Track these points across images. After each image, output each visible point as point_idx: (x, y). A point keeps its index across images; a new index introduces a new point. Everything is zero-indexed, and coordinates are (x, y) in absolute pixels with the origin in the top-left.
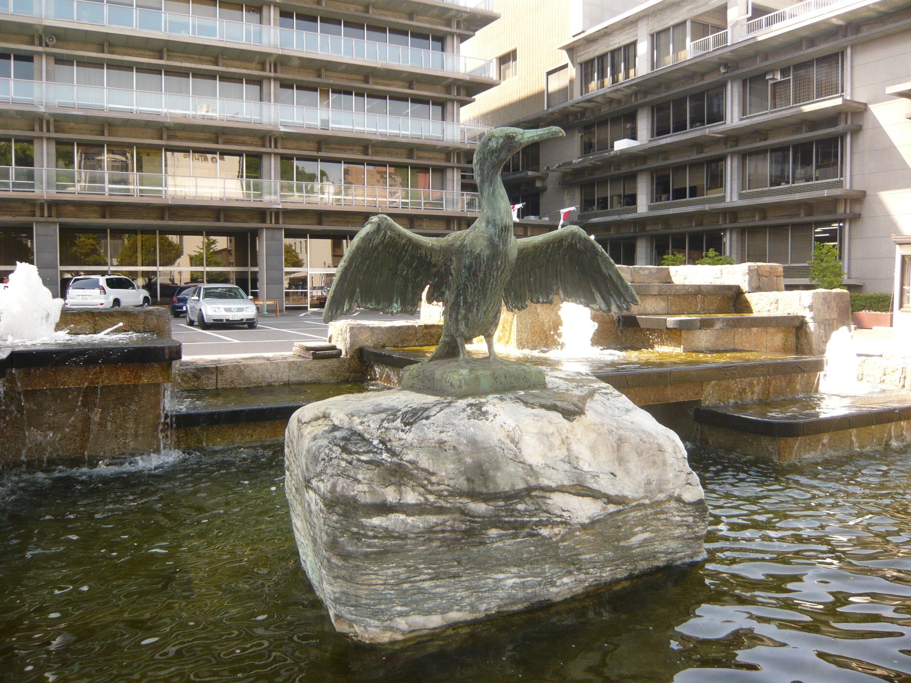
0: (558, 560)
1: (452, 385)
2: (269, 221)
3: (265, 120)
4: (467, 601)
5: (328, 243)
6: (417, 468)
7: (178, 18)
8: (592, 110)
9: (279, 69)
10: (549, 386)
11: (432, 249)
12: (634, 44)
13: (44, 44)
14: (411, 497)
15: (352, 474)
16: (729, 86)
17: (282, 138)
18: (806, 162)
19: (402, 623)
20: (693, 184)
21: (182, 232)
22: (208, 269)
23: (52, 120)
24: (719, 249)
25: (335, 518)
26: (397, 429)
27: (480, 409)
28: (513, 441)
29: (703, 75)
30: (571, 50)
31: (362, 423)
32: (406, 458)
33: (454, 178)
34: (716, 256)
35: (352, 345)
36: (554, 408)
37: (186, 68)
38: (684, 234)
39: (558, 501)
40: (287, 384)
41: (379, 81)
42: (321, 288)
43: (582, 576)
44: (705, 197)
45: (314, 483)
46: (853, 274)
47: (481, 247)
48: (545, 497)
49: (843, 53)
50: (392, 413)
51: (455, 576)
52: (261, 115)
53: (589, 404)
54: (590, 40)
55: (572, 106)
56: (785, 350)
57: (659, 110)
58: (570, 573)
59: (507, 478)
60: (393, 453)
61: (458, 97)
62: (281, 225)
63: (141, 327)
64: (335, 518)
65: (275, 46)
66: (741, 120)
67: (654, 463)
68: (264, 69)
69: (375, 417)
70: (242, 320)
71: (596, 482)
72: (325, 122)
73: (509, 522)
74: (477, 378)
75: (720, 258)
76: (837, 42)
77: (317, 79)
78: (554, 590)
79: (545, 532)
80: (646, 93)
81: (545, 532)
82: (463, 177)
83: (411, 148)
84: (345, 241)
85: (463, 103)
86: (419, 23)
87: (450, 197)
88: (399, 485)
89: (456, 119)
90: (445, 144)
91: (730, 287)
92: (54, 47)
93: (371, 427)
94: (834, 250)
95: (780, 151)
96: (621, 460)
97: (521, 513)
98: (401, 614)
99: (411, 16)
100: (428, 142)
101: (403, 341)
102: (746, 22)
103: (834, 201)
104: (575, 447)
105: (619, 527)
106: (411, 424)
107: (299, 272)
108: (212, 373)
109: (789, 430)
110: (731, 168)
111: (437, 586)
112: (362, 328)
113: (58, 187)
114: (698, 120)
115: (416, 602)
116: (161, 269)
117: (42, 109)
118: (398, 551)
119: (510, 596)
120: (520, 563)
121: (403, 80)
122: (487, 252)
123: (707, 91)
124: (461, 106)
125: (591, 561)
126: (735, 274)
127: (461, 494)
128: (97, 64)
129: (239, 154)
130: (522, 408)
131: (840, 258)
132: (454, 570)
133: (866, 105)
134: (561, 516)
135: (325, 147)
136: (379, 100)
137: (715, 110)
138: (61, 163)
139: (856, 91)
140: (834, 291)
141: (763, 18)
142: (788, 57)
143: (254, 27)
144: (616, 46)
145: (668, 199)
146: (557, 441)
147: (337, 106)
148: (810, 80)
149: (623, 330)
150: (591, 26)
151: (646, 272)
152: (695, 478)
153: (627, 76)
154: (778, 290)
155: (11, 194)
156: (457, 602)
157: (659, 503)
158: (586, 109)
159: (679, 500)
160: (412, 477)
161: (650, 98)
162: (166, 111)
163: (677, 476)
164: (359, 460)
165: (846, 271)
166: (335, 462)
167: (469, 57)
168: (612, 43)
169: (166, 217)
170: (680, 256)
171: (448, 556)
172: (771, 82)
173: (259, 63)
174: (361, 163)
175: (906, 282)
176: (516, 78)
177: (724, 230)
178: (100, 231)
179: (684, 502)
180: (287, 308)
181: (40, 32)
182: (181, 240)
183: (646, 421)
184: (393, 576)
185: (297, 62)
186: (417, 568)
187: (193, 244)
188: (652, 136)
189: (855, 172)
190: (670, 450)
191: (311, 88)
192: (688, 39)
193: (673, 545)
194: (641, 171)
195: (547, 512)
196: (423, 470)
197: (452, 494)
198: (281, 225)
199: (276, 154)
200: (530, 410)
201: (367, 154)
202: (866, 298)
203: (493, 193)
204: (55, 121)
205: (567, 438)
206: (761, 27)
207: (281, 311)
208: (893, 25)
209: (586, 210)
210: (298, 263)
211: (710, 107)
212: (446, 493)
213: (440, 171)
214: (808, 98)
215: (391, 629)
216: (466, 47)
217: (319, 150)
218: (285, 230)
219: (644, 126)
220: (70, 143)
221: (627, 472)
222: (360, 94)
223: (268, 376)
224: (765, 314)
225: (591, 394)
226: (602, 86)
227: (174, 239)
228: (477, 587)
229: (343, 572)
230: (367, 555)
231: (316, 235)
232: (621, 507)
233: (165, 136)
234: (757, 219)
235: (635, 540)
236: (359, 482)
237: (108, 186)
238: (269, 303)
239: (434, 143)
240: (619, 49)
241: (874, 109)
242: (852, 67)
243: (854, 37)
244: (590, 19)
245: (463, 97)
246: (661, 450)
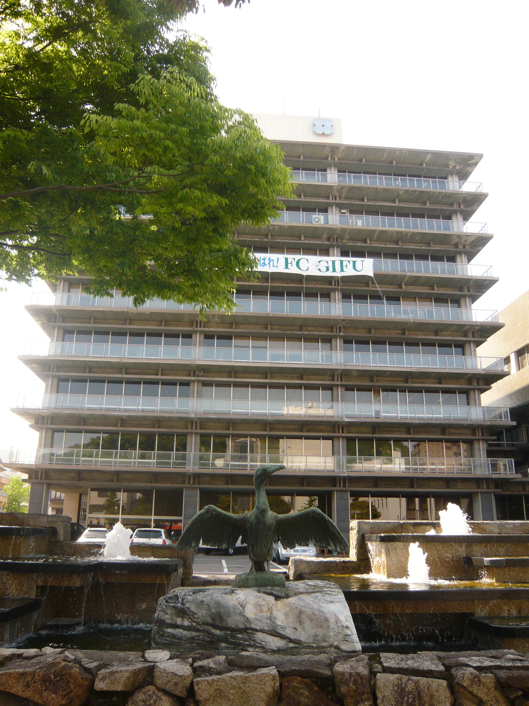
2: (338, 486)
5: (404, 500)
6: (189, 611)
9: (343, 379)
11: (236, 520)
13: (196, 375)
14: (186, 623)
17: (347, 426)
23: (198, 422)
25: (156, 628)
28: (242, 606)
32: (186, 606)
33: (481, 448)
37: (282, 383)
39: (260, 636)
41: (416, 380)
47: (253, 519)
48: (254, 634)
59: (233, 621)
61: (478, 387)
67: (322, 626)
68: (333, 380)
71: (283, 631)
72: (377, 412)
73: (231, 642)
84: (428, 499)
85: (483, 391)
88: (183, 617)
90: (470, 423)
92: (202, 376)
96: (301, 623)
99: (436, 333)
100: (456, 422)
104: (275, 613)
113: (201, 464)
117: (192, 416)
121: (433, 378)
122: (255, 521)
127: (208, 624)
128: (227, 385)
134: (260, 644)
138: (203, 449)
146: (265, 609)
151: (511, 526)
155: (171, 470)
160: (187, 614)
163: (336, 635)
164: (169, 605)
166: (162, 606)
178: (227, 493)
179: (341, 650)
181: (195, 368)
182: (292, 500)
185: (356, 373)
195: (254, 641)
196: (192, 611)
199: (342, 437)
201: (410, 434)
204: (201, 422)
205: (271, 608)
212: (201, 623)
213: (470, 443)
216: (481, 350)
217: (374, 433)
218: (351, 492)
220: (209, 436)
221: (304, 629)
232: (297, 645)
233: (268, 429)
239: (460, 422)
246: (326, 620)
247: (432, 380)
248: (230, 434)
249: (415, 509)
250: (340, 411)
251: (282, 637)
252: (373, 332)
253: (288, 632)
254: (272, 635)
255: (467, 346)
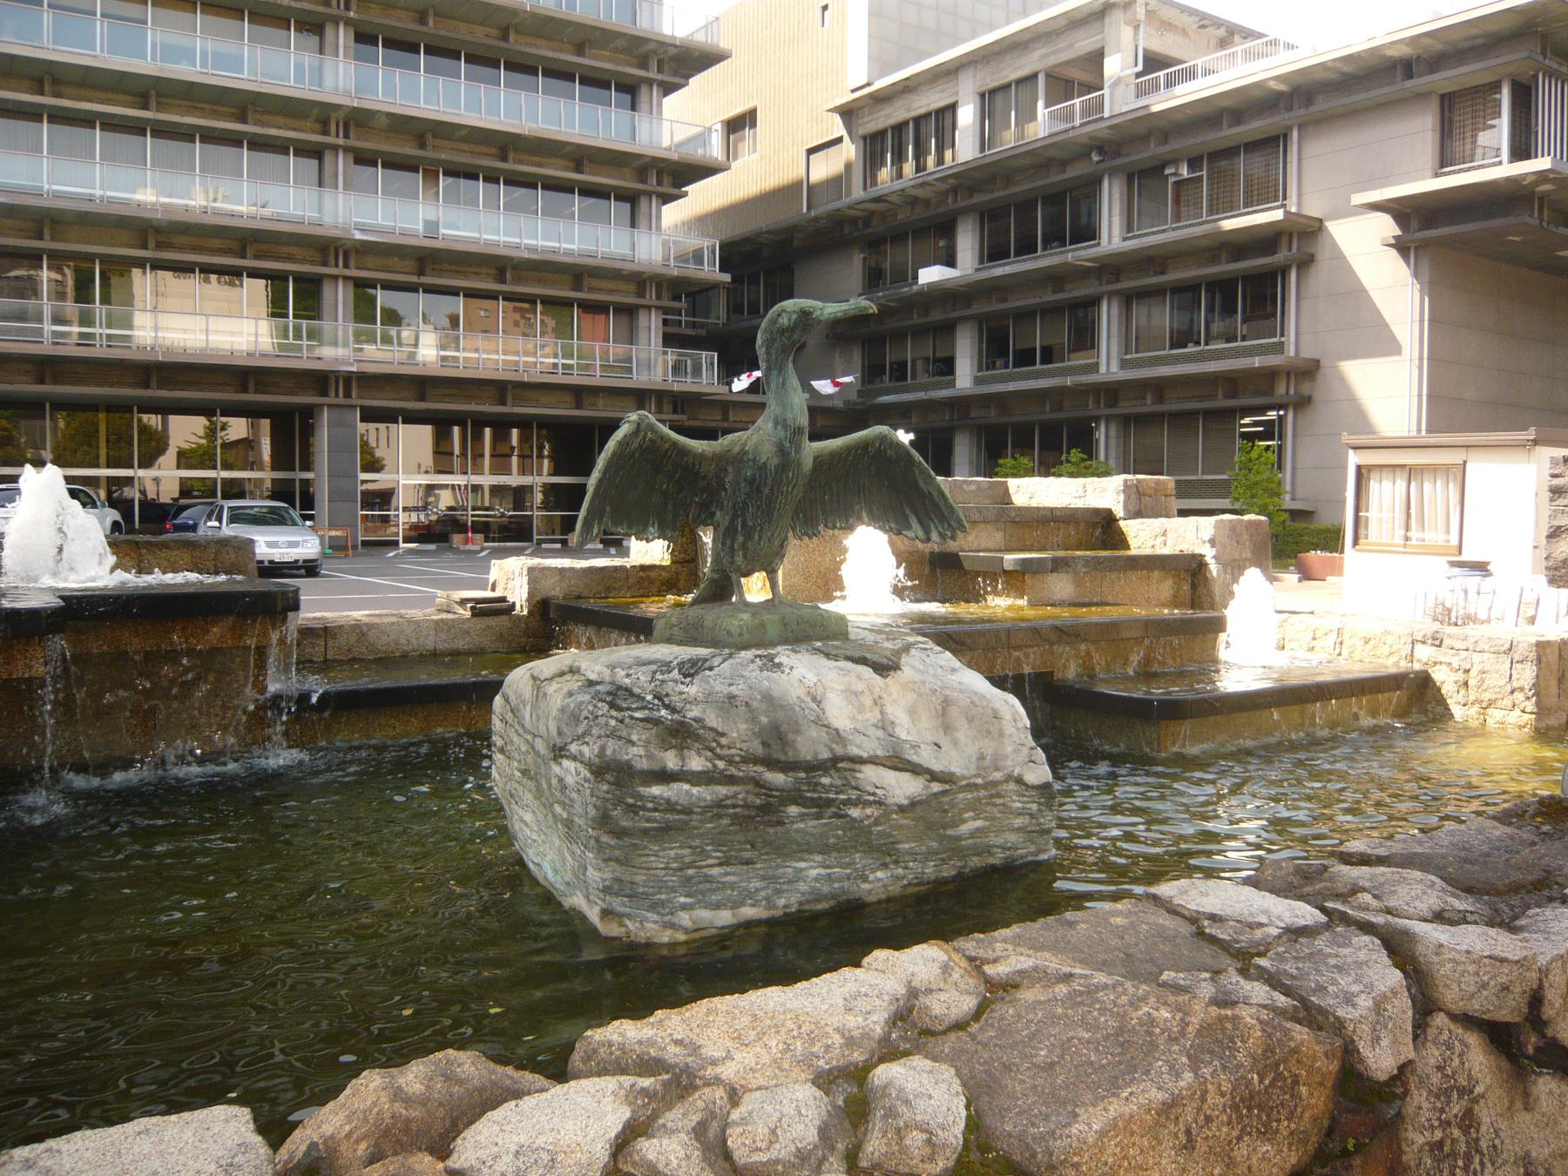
0: (871, 849)
1: (729, 633)
2: (333, 393)
3: (328, 219)
4: (763, 893)
5: (425, 432)
6: (704, 727)
7: (177, 39)
8: (882, 215)
10: (852, 637)
11: (702, 456)
12: (953, 107)
14: (696, 763)
15: (624, 734)
16: (1106, 184)
18: (1229, 309)
19: (685, 919)
20: (1047, 343)
21: (167, 409)
22: (225, 474)
24: (1089, 449)
25: (605, 787)
26: (676, 681)
27: (772, 660)
28: (814, 699)
29: (1064, 164)
30: (848, 113)
31: (628, 676)
32: (691, 714)
33: (651, 326)
34: (1083, 460)
35: (531, 595)
36: (862, 661)
38: (1032, 424)
39: (871, 775)
40: (435, 654)
42: (416, 509)
43: (900, 871)
44: (1066, 364)
45: (574, 748)
46: (1300, 493)
47: (768, 454)
49: (1285, 136)
50: (666, 666)
51: (748, 862)
52: (320, 211)
53: (904, 659)
54: (881, 99)
55: (850, 207)
56: (1175, 603)
57: (991, 218)
58: (885, 866)
59: (811, 744)
60: (673, 710)
61: (659, 189)
62: (354, 400)
63: (210, 565)
64: (605, 787)
65: (347, 94)
66: (1125, 239)
67: (989, 732)
68: (326, 132)
69: (644, 669)
70: (297, 561)
71: (916, 753)
72: (432, 226)
74: (762, 625)
75: (1089, 466)
76: (1277, 118)
77: (419, 152)
78: (865, 886)
79: (855, 813)
80: (972, 190)
81: (855, 813)
82: (665, 322)
83: (578, 274)
85: (667, 199)
86: (592, 61)
87: (643, 355)
88: (681, 749)
89: (654, 224)
90: (636, 268)
91: (1097, 511)
93: (641, 680)
94: (1270, 454)
95: (1186, 293)
96: (947, 728)
97: (827, 789)
98: (684, 907)
100: (608, 264)
101: (608, 589)
102: (1133, 80)
103: (1271, 375)
104: (889, 710)
105: (945, 811)
106: (692, 675)
107: (381, 480)
108: (319, 637)
109: (1173, 711)
110: (1108, 318)
111: (727, 874)
112: (544, 570)
114: (1055, 238)
115: (700, 890)
116: (141, 473)
118: (681, 828)
119: (813, 891)
120: (825, 850)
122: (775, 462)
123: (1071, 190)
124: (665, 203)
125: (911, 853)
126: (1102, 492)
127: (756, 761)
129: (254, 274)
130: (823, 661)
131: (1280, 468)
132: (747, 855)
133: (1320, 221)
134: (874, 794)
135: (430, 268)
136: (524, 190)
137: (1084, 220)
139: (1306, 198)
140: (1247, 517)
141: (1161, 73)
142: (1199, 139)
143: (309, 59)
144: (923, 111)
145: (1006, 367)
146: (868, 702)
147: (452, 198)
148: (1234, 175)
149: (938, 572)
150: (882, 76)
151: (973, 487)
152: (1040, 755)
153: (940, 160)
154: (1168, 516)
156: (750, 895)
157: (995, 783)
158: (872, 213)
159: (1019, 781)
160: (698, 738)
161: (978, 199)
162: (153, 199)
164: (632, 717)
165: (1288, 487)
166: (602, 720)
167: (680, 119)
168: (915, 105)
169: (154, 383)
170: (1025, 461)
171: (740, 837)
172: (1172, 180)
173: (317, 121)
174: (492, 296)
175: (1363, 507)
176: (754, 156)
177: (1097, 419)
180: (365, 543)
182: (165, 423)
183: (977, 682)
184: (678, 858)
185: (384, 121)
186: (703, 851)
187: (186, 430)
188: (981, 262)
189: (1303, 328)
190: (1008, 716)
191: (409, 166)
192: (1040, 104)
193: (1012, 838)
194: (964, 319)
196: (711, 729)
197: (745, 760)
198: (354, 400)
199: (346, 278)
200: (833, 663)
201: (503, 282)
202: (1319, 532)
203: (784, 383)
206: (1158, 88)
207: (355, 547)
208: (1364, 96)
209: (870, 382)
210: (373, 465)
211: (1076, 215)
213: (628, 312)
214: (1230, 208)
215: (672, 926)
216: (672, 103)
217: (421, 273)
219: (967, 244)
221: (955, 743)
222: (492, 178)
223: (403, 641)
224: (1147, 551)
225: (907, 648)
226: (900, 176)
227: (153, 420)
228: (774, 877)
229: (617, 853)
230: (645, 832)
231: (412, 418)
233: (151, 244)
234: (1149, 401)
235: (965, 828)
236: (633, 744)
237: (48, 327)
238: (333, 533)
239: (618, 265)
240: (927, 115)
241: (1331, 226)
242: (1299, 160)
243: (1303, 111)
244: (880, 63)
245: (667, 189)
246: (997, 716)
247: (560, 162)
248: (43, 250)
249: (452, 454)
250: (341, 213)
251: (916, 770)
252: (431, 23)
253: (926, 757)
254: (895, 768)
255: (644, 90)
